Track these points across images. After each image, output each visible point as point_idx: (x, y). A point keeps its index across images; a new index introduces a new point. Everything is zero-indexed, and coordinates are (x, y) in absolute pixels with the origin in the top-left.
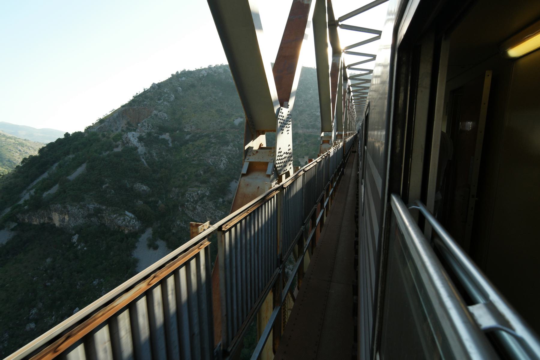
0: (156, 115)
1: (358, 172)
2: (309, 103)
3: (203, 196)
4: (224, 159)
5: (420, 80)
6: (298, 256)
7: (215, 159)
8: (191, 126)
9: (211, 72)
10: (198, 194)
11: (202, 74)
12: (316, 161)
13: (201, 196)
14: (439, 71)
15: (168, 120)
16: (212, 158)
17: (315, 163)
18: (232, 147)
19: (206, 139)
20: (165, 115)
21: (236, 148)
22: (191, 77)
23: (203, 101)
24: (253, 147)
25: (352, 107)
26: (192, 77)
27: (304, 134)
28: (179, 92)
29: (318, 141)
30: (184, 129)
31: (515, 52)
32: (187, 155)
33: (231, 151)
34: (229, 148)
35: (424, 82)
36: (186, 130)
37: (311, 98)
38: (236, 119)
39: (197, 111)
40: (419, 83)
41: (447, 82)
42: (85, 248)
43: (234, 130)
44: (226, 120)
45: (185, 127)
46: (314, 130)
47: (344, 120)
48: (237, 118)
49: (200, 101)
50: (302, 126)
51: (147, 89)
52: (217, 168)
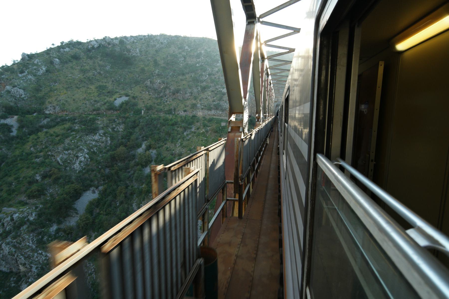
0: (9, 92)
1: (279, 146)
2: (215, 78)
3: (22, 222)
4: (81, 154)
5: (338, 60)
6: (247, 184)
7: (70, 154)
8: (54, 106)
9: (105, 43)
10: (12, 219)
11: (91, 45)
12: (259, 128)
13: (17, 223)
14: (354, 53)
15: (25, 99)
16: (65, 154)
17: (258, 129)
18: (100, 136)
19: (68, 125)
20: (21, 92)
21: (107, 137)
22: (78, 49)
23: (83, 76)
24: (232, 120)
25: (272, 94)
26: (80, 49)
27: (204, 117)
28: (56, 64)
29: (221, 128)
30: (44, 111)
31: (401, 46)
32: (32, 149)
33: (98, 142)
34: (97, 137)
35: (342, 61)
36: (47, 112)
37: (217, 72)
38: (119, 98)
39: (71, 87)
40: (338, 62)
41: (359, 65)
42: (34, 221)
43: (112, 111)
44: (105, 99)
45: (46, 108)
46: (218, 112)
47: (270, 106)
48: (121, 97)
49: (79, 76)
50: (202, 107)
51: (18, 61)
52: (68, 168)
